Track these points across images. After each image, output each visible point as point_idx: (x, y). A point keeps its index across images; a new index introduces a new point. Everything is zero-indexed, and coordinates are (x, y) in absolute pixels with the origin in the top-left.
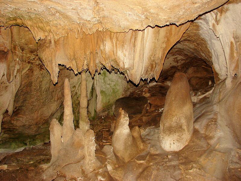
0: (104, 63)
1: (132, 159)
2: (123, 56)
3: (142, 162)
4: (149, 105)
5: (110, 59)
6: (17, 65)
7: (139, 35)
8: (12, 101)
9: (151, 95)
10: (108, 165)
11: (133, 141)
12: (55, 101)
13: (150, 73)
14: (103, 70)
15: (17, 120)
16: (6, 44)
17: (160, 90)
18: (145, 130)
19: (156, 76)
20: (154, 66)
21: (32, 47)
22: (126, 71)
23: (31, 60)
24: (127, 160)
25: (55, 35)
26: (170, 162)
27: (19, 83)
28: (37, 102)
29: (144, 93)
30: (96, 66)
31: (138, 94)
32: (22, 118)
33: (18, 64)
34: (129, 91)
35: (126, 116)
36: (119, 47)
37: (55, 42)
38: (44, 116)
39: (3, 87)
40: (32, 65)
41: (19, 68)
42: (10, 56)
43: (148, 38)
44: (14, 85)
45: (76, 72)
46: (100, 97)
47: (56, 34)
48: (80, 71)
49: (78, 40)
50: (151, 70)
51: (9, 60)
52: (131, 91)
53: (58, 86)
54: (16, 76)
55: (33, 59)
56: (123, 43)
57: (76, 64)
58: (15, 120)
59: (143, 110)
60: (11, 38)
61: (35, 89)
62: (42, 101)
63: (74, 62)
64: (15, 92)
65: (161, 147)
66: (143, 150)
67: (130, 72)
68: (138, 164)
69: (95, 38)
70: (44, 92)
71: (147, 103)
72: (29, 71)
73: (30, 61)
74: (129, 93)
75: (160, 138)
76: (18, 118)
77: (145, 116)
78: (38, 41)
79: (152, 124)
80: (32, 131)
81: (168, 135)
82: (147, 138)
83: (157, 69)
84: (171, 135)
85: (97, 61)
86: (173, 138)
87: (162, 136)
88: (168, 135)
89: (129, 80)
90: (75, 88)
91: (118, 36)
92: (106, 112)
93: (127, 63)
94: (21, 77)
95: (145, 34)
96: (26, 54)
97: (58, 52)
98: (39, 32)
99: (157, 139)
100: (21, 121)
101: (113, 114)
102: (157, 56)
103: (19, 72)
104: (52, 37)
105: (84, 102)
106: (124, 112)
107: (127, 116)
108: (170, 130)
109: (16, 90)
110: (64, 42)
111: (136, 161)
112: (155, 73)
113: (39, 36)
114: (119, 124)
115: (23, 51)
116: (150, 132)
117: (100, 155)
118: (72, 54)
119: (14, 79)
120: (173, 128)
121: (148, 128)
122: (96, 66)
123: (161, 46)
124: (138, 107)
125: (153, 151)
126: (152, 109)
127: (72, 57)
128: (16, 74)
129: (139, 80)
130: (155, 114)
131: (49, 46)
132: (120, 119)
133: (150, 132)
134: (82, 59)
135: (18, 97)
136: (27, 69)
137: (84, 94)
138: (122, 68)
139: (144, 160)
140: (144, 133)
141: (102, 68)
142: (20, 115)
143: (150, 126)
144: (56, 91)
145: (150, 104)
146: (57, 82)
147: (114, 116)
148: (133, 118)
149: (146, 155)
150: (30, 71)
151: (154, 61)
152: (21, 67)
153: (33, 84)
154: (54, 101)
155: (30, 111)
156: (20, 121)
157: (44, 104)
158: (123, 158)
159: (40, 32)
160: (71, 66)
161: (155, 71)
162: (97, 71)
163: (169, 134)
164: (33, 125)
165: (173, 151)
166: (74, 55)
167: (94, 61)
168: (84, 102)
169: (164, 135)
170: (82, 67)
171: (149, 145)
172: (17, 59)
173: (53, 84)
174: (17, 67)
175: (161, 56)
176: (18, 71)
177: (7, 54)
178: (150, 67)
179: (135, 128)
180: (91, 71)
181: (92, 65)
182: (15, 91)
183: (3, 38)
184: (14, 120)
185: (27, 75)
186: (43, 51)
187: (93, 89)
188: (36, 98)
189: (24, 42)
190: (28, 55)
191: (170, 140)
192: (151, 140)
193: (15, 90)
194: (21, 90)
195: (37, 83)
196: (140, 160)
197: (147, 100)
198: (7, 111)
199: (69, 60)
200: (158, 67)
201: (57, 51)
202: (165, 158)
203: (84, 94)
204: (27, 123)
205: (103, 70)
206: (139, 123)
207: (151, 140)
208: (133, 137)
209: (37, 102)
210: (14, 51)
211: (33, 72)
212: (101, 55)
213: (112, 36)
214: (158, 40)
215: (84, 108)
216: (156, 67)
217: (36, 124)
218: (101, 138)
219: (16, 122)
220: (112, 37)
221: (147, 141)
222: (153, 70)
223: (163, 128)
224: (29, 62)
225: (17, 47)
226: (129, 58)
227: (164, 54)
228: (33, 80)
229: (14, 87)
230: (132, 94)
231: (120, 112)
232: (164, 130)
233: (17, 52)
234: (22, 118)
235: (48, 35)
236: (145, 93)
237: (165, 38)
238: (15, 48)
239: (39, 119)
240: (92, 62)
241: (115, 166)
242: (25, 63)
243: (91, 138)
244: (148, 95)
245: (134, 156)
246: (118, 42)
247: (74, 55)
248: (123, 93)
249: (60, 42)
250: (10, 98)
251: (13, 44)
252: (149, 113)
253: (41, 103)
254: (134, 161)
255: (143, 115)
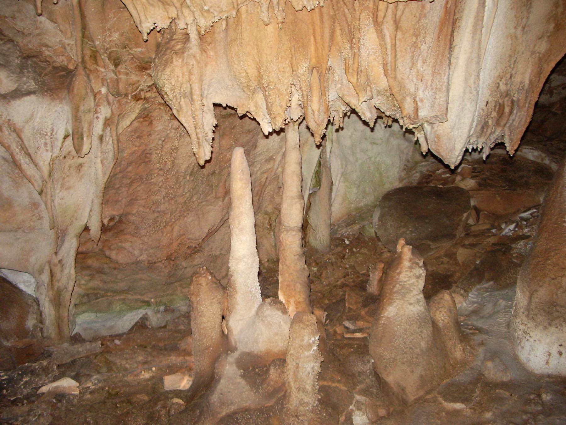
0: (354, 103)
1: (429, 392)
2: (415, 80)
3: (458, 406)
4: (474, 213)
5: (371, 88)
6: (102, 107)
7: (466, 12)
8: (97, 202)
9: (480, 185)
10: (358, 413)
11: (434, 339)
12: (219, 198)
13: (494, 132)
14: (349, 117)
15: (120, 249)
16: (68, 48)
17: (503, 170)
18: (468, 296)
19: (511, 140)
20: (507, 110)
21: (141, 53)
22: (422, 125)
23: (142, 90)
24: (411, 395)
25: (197, 14)
26: (550, 415)
27: (111, 155)
28: (167, 205)
29: (458, 178)
30: (328, 109)
31: (443, 179)
32: (131, 242)
33: (106, 103)
34: (419, 169)
35: (417, 264)
36: (401, 51)
37: (201, 37)
38: (189, 239)
39: (70, 167)
40: (147, 105)
41: (109, 115)
42: (79, 82)
43: (496, 21)
44: (99, 160)
45: (267, 129)
46: (339, 187)
47: (202, 10)
48: (279, 125)
49: (270, 28)
50: (498, 124)
51: (75, 92)
52: (424, 170)
53: (212, 174)
54: (101, 138)
55: (149, 87)
56: (417, 36)
57: (267, 105)
58: (112, 247)
59: (459, 227)
60: (79, 28)
61: (161, 170)
62: (181, 200)
63: (260, 97)
64: (102, 180)
65: (516, 358)
66: (464, 363)
67: (432, 128)
68: (447, 413)
69: (324, 20)
70: (185, 178)
71: (466, 207)
72: (142, 120)
73: (140, 93)
74: (418, 175)
75: (515, 330)
76: (120, 244)
77: (464, 246)
78: (148, 34)
79: (487, 275)
80: (160, 276)
81: (541, 327)
82: (475, 323)
83: (513, 120)
84: (553, 329)
85: (332, 95)
86: (558, 339)
87: (522, 327)
88: (541, 327)
89: (429, 149)
90: (272, 163)
91: (399, 13)
92: (356, 227)
93: (425, 101)
94: (115, 138)
95: (486, 8)
96: (127, 74)
97: (209, 67)
98: (151, 8)
99: (504, 330)
100: (129, 252)
101: (374, 234)
102: (517, 79)
103: (109, 125)
104: (190, 20)
105: (292, 215)
106: (413, 253)
107: (421, 264)
108: (549, 313)
109: (104, 174)
110: (226, 36)
111: (441, 399)
112: (507, 133)
113: (151, 21)
114: (394, 287)
115: (116, 65)
116: (482, 305)
117: (333, 382)
118: (252, 72)
119: (94, 147)
120: (562, 306)
121: (474, 289)
122: (328, 109)
123: (534, 47)
124: (445, 220)
125: (493, 371)
126: (484, 226)
127: (254, 84)
128: (103, 130)
129: (462, 154)
130: (492, 240)
131: (183, 51)
132: (399, 273)
133: (482, 305)
134: (282, 88)
135: (114, 191)
136: (133, 116)
137: (292, 186)
138: (409, 118)
139: (464, 401)
140: (464, 304)
141: (348, 114)
142: (125, 234)
143: (480, 282)
144: (219, 173)
145: (477, 211)
146: (208, 158)
147: (376, 239)
148: (431, 250)
149: (470, 383)
150: (141, 122)
151: (506, 96)
152: (114, 111)
153: (154, 157)
154: (217, 198)
155: (150, 226)
156: (126, 251)
157: (187, 208)
158: (403, 390)
159: (153, 5)
160: (252, 109)
161: (508, 125)
162: (332, 124)
163: (546, 323)
164: (161, 261)
165: (555, 373)
166: (260, 77)
167: (323, 93)
168: (292, 215)
169: (531, 324)
170: (283, 114)
171: (481, 351)
172: (104, 90)
173: (199, 164)
174: (105, 112)
175: (531, 82)
176: (108, 122)
177: (72, 78)
178: (494, 114)
179: (441, 296)
180: (312, 125)
181: (315, 105)
182: (104, 176)
183: (62, 32)
184: (110, 249)
185: (135, 131)
186: (166, 64)
187: (322, 166)
188: (163, 193)
189: (118, 39)
190: (134, 78)
191: (548, 341)
192: (487, 332)
193: (101, 175)
194: (120, 172)
195: (164, 153)
196: (455, 400)
197: (469, 197)
198: (86, 229)
199: (244, 91)
200: (519, 114)
201: (206, 64)
202: (530, 400)
203: (292, 186)
204: (144, 257)
205: (349, 117)
206: (446, 266)
207: (487, 332)
208: (434, 324)
209: (167, 205)
210: (93, 67)
211: (151, 123)
212: (345, 77)
213: (381, 14)
214: (524, 28)
215: (292, 229)
216: (511, 112)
217: (169, 258)
218: (339, 314)
219: (117, 254)
220: (380, 19)
221: (476, 337)
222: (502, 124)
223: (526, 303)
224: (137, 98)
225: (98, 54)
226: (434, 85)
227: (540, 73)
228: (152, 145)
229: (99, 166)
230: (427, 178)
231: (399, 248)
232: (528, 309)
233: (103, 70)
234: (131, 242)
235: (178, 16)
236: (463, 179)
237: (548, 20)
238: (95, 57)
239: (175, 246)
240: (315, 98)
241: (376, 413)
242: (125, 100)
243: (306, 338)
244: (469, 184)
245: (434, 383)
246: (399, 34)
247: (260, 77)
248: (403, 174)
249: (216, 35)
250: (91, 196)
251: (88, 45)
252: (475, 236)
253: (180, 206)
254: (435, 401)
255: (456, 244)
